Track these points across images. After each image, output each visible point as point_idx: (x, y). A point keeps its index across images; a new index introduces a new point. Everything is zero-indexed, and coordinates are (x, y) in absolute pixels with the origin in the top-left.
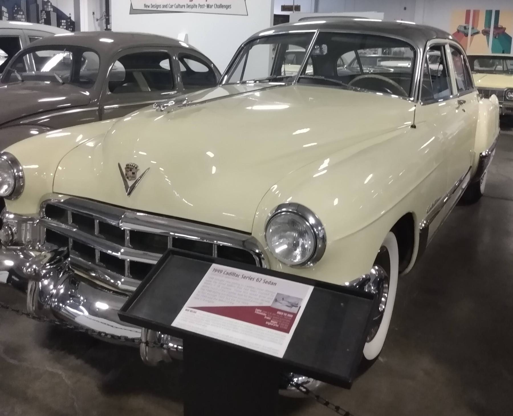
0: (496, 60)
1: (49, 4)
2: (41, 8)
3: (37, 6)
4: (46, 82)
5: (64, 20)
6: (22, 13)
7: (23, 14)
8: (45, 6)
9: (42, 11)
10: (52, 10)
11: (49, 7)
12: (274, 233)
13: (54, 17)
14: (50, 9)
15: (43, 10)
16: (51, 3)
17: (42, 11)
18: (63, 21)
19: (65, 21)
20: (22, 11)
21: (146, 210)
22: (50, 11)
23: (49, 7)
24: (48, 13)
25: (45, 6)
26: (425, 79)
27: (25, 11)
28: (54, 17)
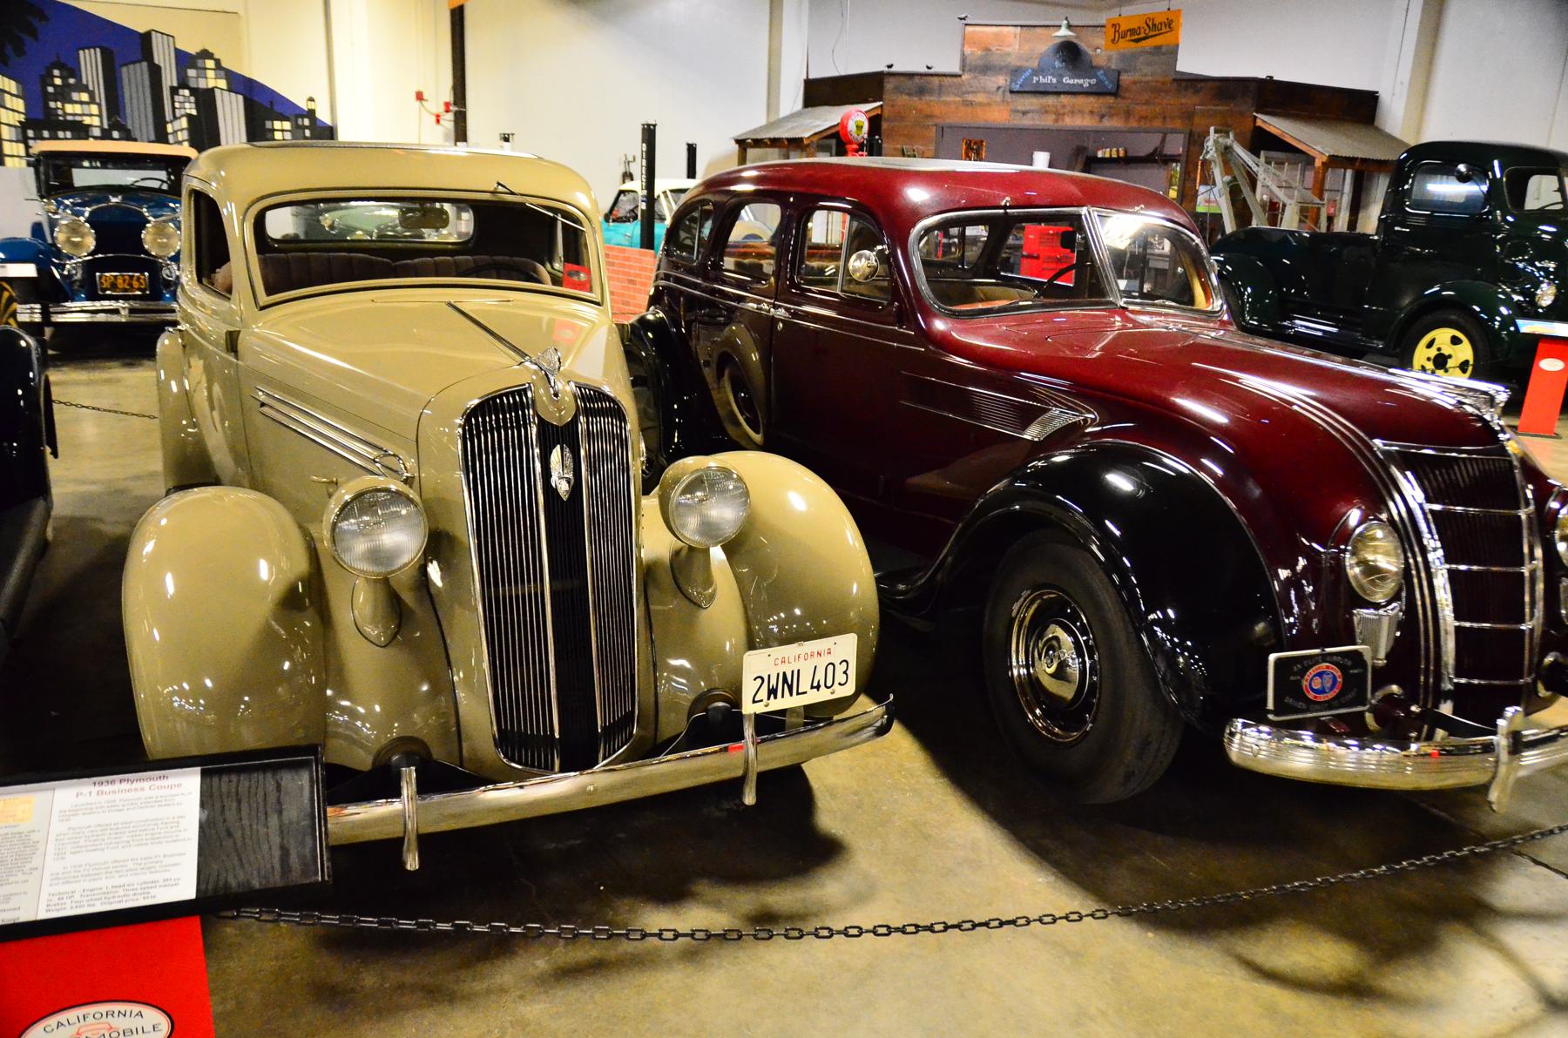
0: (225, 778)
1: (210, 64)
2: (169, 78)
3: (155, 72)
4: (1065, 458)
5: (283, 118)
6: (85, 97)
7: (92, 101)
8: (191, 73)
9: (174, 91)
10: (222, 84)
11: (211, 74)
12: (1482, 839)
13: (231, 114)
14: (212, 80)
15: (183, 83)
16: (218, 62)
17: (174, 91)
18: (277, 125)
19: (287, 125)
20: (85, 89)
21: (41, 943)
22: (211, 92)
23: (211, 74)
24: (205, 99)
25: (191, 73)
26: (557, 768)
27: (101, 95)
28: (231, 114)
